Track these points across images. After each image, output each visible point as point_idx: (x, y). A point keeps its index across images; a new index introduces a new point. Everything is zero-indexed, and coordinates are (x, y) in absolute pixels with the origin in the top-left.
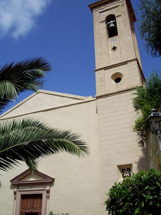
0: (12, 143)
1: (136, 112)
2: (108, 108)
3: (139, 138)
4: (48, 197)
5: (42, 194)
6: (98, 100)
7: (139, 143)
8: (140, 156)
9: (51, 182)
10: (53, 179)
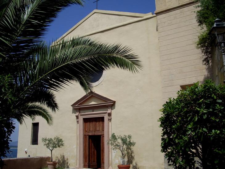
0: (60, 62)
1: (200, 28)
2: (169, 25)
3: (204, 56)
4: (110, 120)
5: (103, 117)
6: (158, 17)
7: (203, 61)
8: (205, 75)
9: (112, 104)
10: (114, 102)
